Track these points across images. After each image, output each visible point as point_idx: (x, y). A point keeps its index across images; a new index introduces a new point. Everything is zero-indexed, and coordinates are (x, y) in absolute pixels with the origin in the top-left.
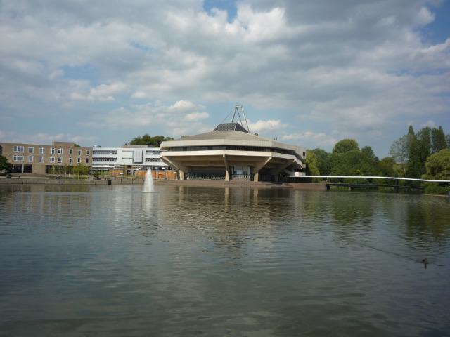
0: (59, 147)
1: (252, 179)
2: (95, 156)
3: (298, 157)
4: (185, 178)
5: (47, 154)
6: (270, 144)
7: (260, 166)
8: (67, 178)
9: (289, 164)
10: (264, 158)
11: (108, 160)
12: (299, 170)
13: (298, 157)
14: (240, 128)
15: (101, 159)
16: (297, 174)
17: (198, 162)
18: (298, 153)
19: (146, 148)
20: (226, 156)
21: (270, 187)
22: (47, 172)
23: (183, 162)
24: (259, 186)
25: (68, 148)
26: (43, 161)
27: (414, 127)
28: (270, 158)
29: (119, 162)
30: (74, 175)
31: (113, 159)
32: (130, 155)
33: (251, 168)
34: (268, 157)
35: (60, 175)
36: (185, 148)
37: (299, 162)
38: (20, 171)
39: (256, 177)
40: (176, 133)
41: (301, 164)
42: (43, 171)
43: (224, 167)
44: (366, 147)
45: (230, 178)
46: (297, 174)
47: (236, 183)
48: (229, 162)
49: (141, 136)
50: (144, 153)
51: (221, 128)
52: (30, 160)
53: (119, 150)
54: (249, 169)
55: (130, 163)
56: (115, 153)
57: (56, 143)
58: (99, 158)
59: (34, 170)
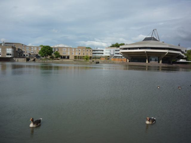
0: (79, 49)
1: (159, 62)
2: (94, 52)
3: (183, 52)
4: (129, 61)
5: (75, 51)
6: (167, 47)
7: (163, 57)
8: (80, 61)
9: (178, 56)
10: (165, 53)
11: (101, 53)
12: (183, 58)
13: (183, 52)
14: (155, 39)
15: (99, 53)
16: (181, 60)
17: (134, 54)
18: (182, 51)
19: (115, 48)
20: (147, 52)
21: (167, 66)
22: (75, 59)
23: (129, 54)
24: (162, 66)
25: (83, 49)
26: (73, 54)
27: (34, 119)
28: (167, 53)
29: (105, 55)
30: (83, 60)
31: (103, 53)
32: (108, 52)
33: (158, 57)
34: (166, 52)
35: (80, 60)
36: (129, 49)
37: (183, 55)
38: (65, 58)
39: (161, 62)
40: (128, 43)
41: (184, 56)
42: (73, 58)
43: (146, 57)
44: (48, 47)
45: (149, 62)
46: (181, 60)
47: (151, 64)
48: (148, 54)
49: (115, 43)
50: (115, 51)
51: (146, 39)
52: (68, 54)
53: (104, 50)
54: (157, 58)
55: (108, 55)
56: (103, 51)
57: (78, 47)
58: (100, 53)
59: (70, 58)
